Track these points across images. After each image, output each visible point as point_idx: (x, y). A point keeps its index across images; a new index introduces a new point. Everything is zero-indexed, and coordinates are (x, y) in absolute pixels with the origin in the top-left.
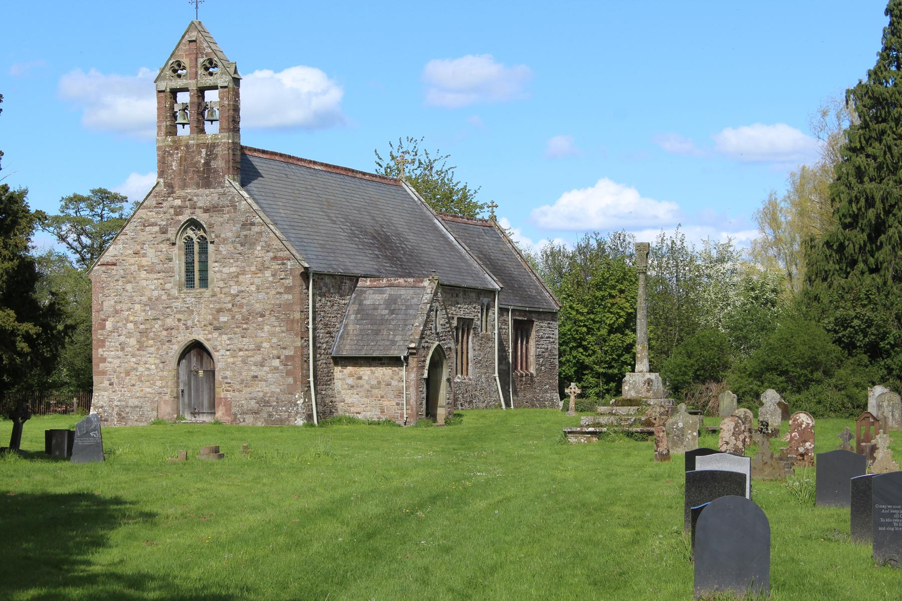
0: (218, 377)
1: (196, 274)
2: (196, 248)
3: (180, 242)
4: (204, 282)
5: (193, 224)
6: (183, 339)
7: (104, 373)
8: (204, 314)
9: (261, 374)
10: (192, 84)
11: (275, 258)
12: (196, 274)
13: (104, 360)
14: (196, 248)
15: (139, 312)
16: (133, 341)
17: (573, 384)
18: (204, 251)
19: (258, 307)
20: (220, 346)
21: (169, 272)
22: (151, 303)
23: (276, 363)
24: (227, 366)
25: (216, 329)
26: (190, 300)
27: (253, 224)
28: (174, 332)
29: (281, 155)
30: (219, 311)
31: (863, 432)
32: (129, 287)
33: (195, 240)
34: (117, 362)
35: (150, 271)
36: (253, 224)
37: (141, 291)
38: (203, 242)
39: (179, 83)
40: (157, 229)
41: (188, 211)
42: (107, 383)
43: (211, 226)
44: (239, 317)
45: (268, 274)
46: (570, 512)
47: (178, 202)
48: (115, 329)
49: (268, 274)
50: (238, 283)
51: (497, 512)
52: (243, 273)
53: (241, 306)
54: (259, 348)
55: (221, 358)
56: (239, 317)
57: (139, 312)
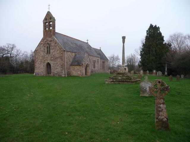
0: (52, 68)
1: (48, 52)
2: (49, 48)
4: (50, 53)
6: (47, 62)
8: (50, 57)
9: (57, 67)
12: (48, 52)
14: (49, 48)
15: (41, 58)
16: (40, 62)
19: (57, 57)
21: (44, 51)
22: (42, 56)
23: (60, 66)
26: (48, 56)
32: (39, 54)
34: (38, 66)
38: (50, 46)
39: (50, 20)
40: (43, 45)
46: (94, 98)
47: (46, 40)
51: (66, 133)
52: (55, 51)
55: (52, 65)
57: (41, 58)
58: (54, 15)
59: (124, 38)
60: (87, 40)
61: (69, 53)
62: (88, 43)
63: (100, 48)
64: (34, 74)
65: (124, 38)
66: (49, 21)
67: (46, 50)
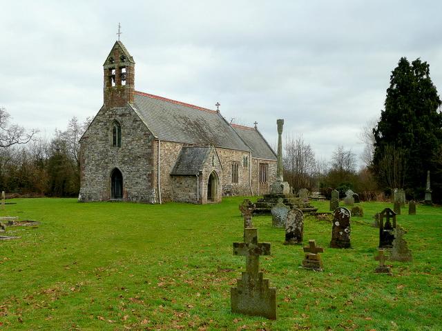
1: (117, 142)
3: (111, 129)
4: (119, 146)
5: (116, 122)
6: (111, 167)
7: (84, 180)
10: (116, 65)
11: (145, 134)
12: (117, 142)
13: (84, 175)
17: (402, 152)
18: (119, 131)
19: (138, 154)
20: (125, 171)
22: (101, 153)
23: (145, 177)
24: (127, 178)
25: (124, 163)
27: (137, 121)
28: (109, 165)
29: (152, 96)
30: (124, 156)
31: (384, 223)
33: (117, 128)
35: (101, 140)
36: (137, 121)
37: (96, 147)
38: (119, 127)
41: (114, 116)
42: (85, 185)
43: (122, 122)
44: (131, 158)
45: (142, 141)
47: (111, 113)
48: (88, 163)
49: (142, 141)
50: (131, 145)
53: (132, 154)
54: (138, 171)
55: (125, 175)
56: (131, 158)
58: (131, 50)
59: (280, 123)
60: (218, 105)
61: (168, 144)
62: (256, 127)
63: (256, 123)
64: (80, 196)
65: (280, 123)
66: (118, 66)
67: (111, 138)
